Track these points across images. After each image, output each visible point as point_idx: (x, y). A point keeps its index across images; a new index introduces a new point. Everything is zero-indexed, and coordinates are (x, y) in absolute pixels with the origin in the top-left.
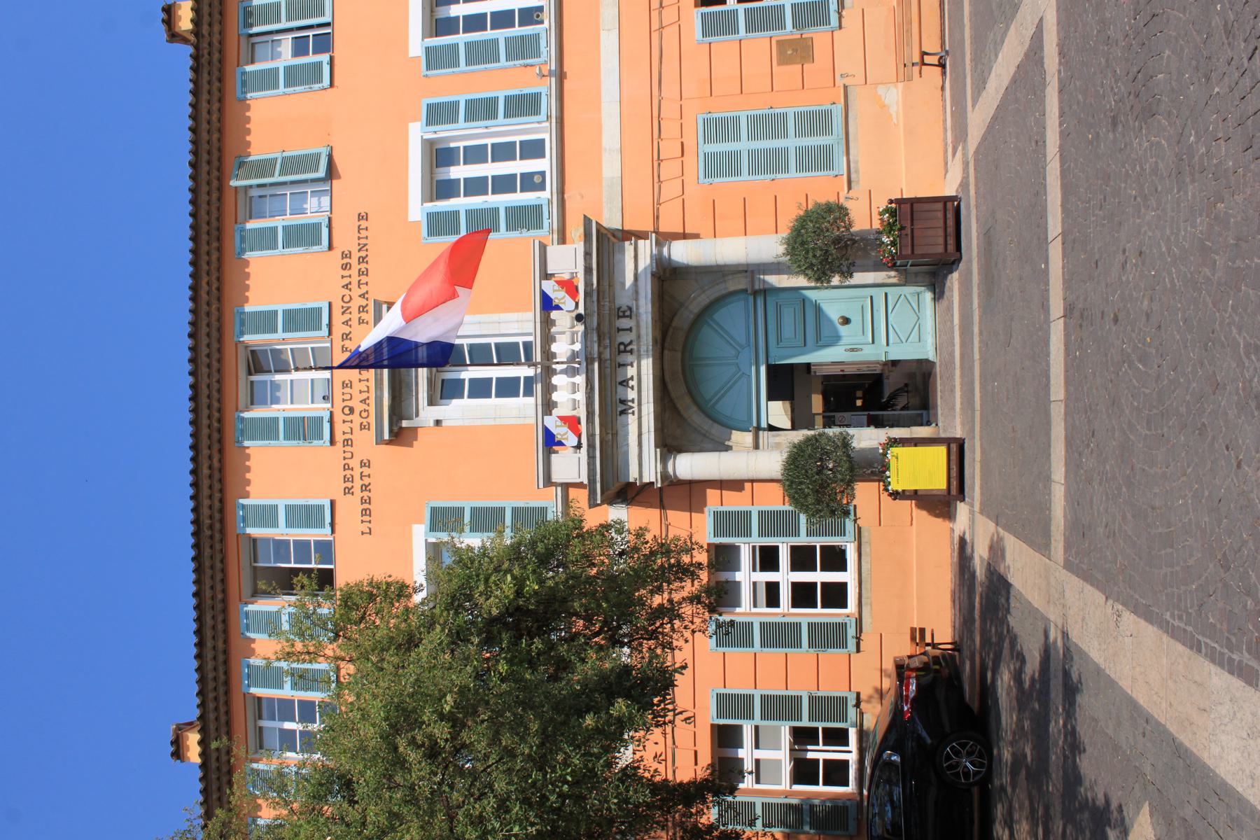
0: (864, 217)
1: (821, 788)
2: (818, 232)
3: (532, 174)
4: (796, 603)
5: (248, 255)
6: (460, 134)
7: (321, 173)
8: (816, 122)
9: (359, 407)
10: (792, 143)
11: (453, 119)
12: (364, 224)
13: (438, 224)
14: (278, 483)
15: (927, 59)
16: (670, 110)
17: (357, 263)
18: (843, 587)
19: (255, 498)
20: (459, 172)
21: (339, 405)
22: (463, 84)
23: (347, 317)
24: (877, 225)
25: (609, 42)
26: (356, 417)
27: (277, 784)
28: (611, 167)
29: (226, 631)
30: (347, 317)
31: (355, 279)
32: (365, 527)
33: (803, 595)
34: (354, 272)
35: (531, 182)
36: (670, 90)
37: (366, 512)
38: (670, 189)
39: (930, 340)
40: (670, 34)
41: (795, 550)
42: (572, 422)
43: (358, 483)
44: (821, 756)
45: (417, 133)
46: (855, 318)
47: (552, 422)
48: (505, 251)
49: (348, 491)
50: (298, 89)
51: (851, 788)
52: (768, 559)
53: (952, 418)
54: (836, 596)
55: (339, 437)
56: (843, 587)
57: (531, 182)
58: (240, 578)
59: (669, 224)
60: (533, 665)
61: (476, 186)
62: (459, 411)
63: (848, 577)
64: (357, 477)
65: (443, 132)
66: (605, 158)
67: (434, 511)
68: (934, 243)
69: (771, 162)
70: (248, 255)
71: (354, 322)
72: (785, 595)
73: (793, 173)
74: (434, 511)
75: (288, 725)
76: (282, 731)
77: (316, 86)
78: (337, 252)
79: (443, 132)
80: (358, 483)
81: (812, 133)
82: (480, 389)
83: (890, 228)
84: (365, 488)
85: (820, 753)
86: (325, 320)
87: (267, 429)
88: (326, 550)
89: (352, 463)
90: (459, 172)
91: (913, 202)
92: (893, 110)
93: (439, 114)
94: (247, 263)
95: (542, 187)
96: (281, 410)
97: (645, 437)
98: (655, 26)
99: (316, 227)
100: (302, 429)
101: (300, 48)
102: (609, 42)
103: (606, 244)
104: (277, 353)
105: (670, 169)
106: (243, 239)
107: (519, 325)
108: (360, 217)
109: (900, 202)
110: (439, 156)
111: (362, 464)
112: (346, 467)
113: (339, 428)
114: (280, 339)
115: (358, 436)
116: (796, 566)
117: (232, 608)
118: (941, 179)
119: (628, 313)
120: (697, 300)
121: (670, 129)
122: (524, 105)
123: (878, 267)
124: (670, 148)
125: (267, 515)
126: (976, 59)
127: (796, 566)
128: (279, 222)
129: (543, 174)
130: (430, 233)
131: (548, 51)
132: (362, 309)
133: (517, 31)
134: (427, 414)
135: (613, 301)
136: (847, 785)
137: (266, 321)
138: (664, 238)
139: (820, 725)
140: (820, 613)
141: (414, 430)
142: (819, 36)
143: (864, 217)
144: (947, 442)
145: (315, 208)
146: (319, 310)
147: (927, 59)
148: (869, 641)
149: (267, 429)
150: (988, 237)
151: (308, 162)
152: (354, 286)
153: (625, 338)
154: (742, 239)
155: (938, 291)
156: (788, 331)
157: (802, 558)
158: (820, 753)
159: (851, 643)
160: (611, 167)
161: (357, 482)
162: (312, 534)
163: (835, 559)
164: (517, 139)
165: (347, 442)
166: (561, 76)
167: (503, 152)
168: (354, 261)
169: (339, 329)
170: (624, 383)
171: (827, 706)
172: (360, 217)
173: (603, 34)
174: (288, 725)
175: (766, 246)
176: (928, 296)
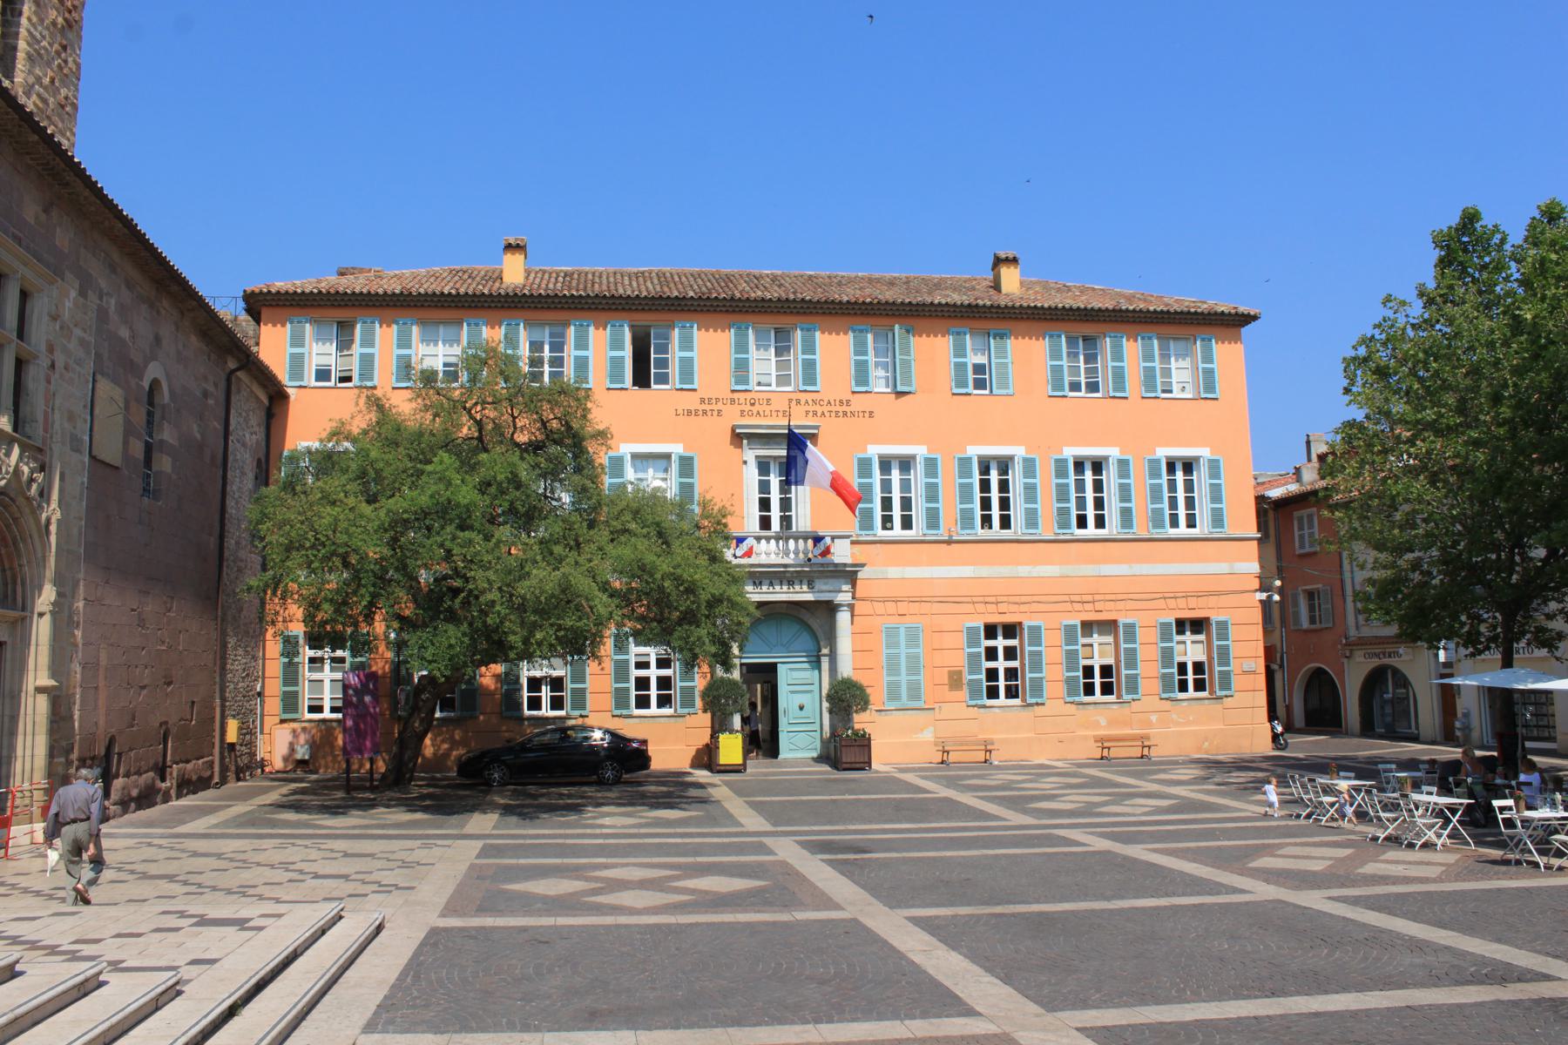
0: (861, 721)
1: (526, 694)
2: (854, 696)
4: (638, 679)
5: (851, 334)
6: (918, 477)
7: (900, 388)
8: (914, 692)
9: (755, 409)
10: (904, 678)
11: (927, 475)
13: (864, 466)
14: (703, 349)
16: (926, 607)
17: (843, 410)
18: (648, 706)
19: (698, 335)
20: (896, 476)
21: (756, 396)
22: (948, 481)
24: (857, 726)
25: (967, 571)
26: (748, 407)
27: (511, 341)
28: (894, 572)
31: (834, 409)
33: (643, 683)
36: (937, 608)
37: (689, 412)
38: (879, 608)
42: (749, 554)
44: (543, 694)
45: (920, 451)
46: (803, 713)
47: (750, 541)
48: (845, 521)
49: (702, 401)
51: (527, 712)
52: (1010, 653)
53: (758, 767)
54: (643, 702)
55: (736, 396)
56: (648, 706)
57: (887, 521)
58: (643, 319)
59: (860, 607)
61: (887, 486)
62: (752, 474)
63: (654, 709)
65: (920, 467)
66: (899, 569)
67: (691, 459)
68: (848, 756)
69: (893, 668)
70: (851, 334)
72: (642, 673)
73: (886, 678)
74: (691, 459)
75: (547, 348)
76: (542, 344)
78: (850, 397)
79: (920, 467)
81: (909, 689)
82: (764, 487)
83: (856, 733)
84: (705, 412)
85: (545, 693)
87: (742, 347)
88: (663, 379)
90: (896, 476)
91: (869, 746)
93: (931, 465)
94: (846, 333)
95: (884, 528)
96: (754, 354)
99: (866, 383)
100: (742, 368)
101: (979, 369)
102: (967, 571)
103: (849, 574)
104: (788, 349)
105: (891, 607)
106: (861, 331)
107: (803, 519)
109: (869, 739)
110: (906, 464)
113: (742, 396)
114: (797, 356)
115: (737, 408)
116: (659, 679)
117: (624, 314)
118: (882, 759)
120: (815, 623)
121: (914, 608)
122: (933, 520)
123: (832, 726)
124: (903, 608)
125: (687, 344)
126: (1004, 798)
127: (659, 679)
128: (871, 357)
131: (965, 535)
132: (815, 413)
133: (978, 513)
134: (750, 455)
137: (809, 347)
138: (851, 607)
141: (741, 446)
142: (964, 694)
143: (861, 721)
144: (744, 765)
145: (879, 381)
149: (742, 347)
150: (853, 780)
151: (907, 381)
154: (849, 654)
155: (820, 759)
156: (796, 674)
157: (664, 683)
158: (545, 693)
159: (618, 712)
160: (894, 572)
161: (707, 408)
162: (674, 370)
163: (664, 701)
164: (913, 513)
165: (733, 401)
166: (949, 542)
169: (803, 397)
170: (771, 584)
171: (579, 699)
174: (547, 348)
175: (846, 669)
176: (815, 755)
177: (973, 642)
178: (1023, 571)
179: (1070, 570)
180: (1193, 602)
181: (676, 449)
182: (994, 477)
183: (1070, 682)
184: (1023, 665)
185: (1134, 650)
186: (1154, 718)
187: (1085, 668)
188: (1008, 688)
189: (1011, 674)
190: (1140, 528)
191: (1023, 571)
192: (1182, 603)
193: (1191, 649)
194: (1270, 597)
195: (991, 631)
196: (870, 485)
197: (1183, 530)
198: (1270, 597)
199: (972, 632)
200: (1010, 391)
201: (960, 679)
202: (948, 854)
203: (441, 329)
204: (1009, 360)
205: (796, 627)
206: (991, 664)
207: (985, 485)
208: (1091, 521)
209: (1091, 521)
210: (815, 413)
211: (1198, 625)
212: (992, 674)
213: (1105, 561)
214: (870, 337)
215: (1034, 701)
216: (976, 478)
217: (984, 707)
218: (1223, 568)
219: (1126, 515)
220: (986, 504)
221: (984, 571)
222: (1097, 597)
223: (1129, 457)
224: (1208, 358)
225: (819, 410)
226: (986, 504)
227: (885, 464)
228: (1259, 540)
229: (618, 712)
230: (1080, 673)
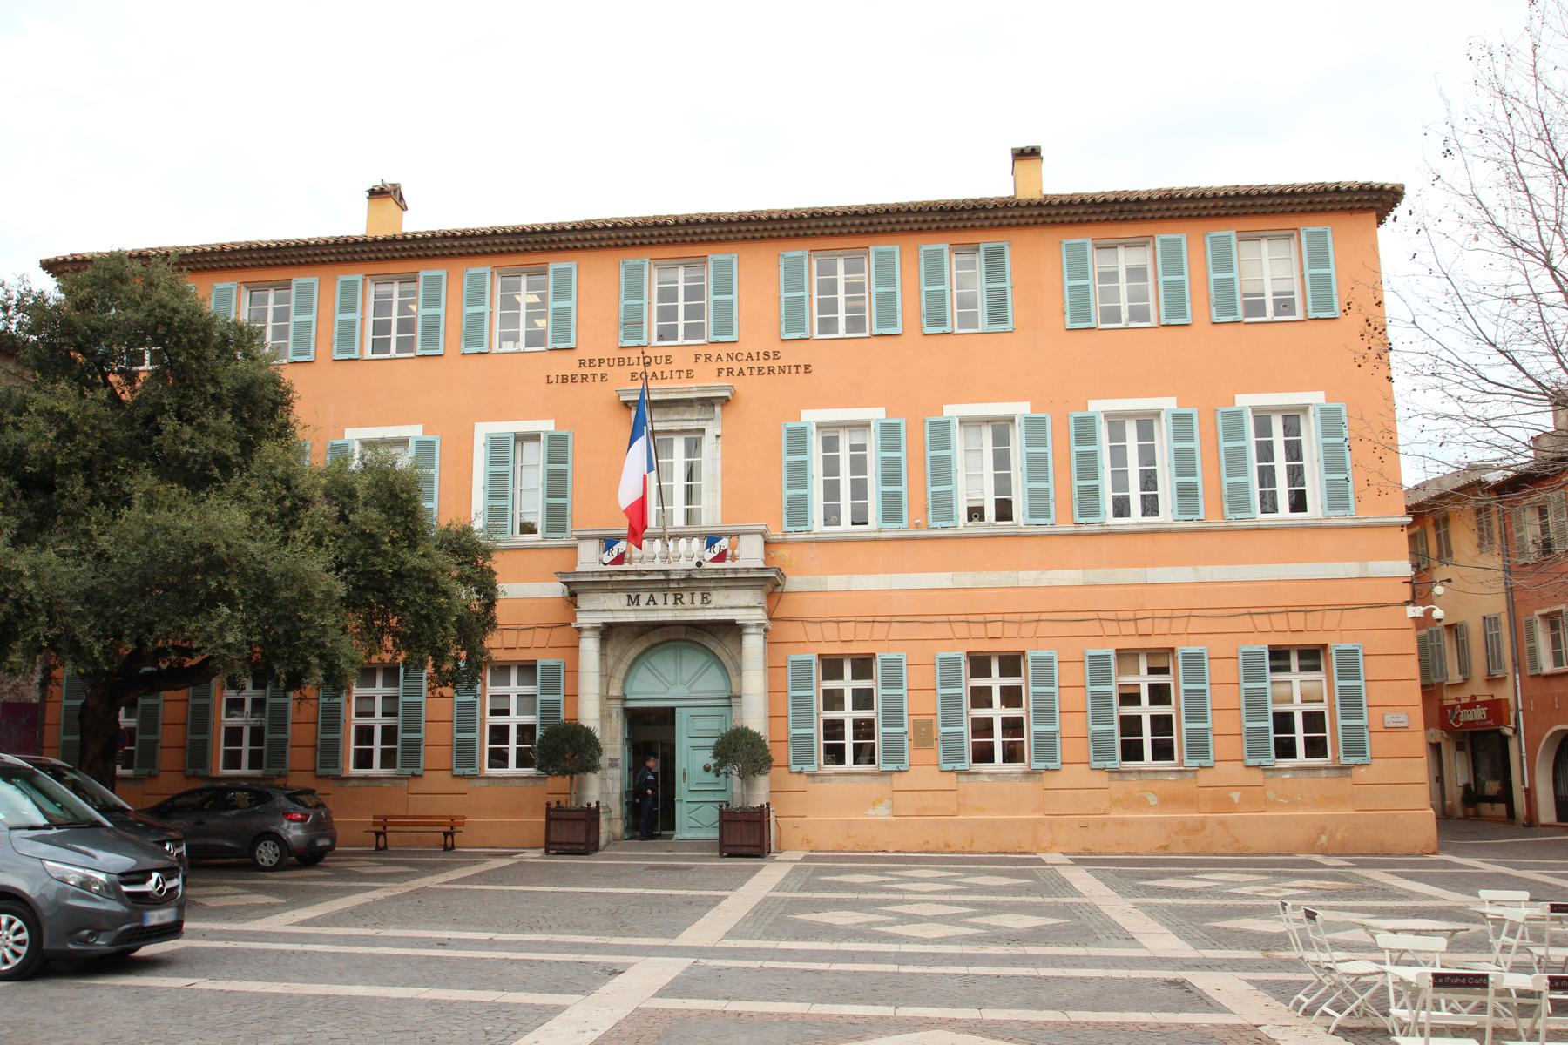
1: (353, 747)
3: (838, 514)
4: (1124, 719)
12: (801, 370)
15: (381, 844)
17: (769, 365)
23: (724, 357)
25: (943, 580)
28: (835, 582)
29: (469, 255)
30: (724, 357)
31: (756, 364)
32: (553, 378)
34: (762, 363)
35: (832, 516)
37: (565, 379)
39: (689, 835)
40: (1095, 628)
41: (870, 723)
43: (588, 371)
49: (582, 363)
50: (924, 304)
52: (1012, 697)
55: (624, 354)
56: (990, 759)
57: (832, 516)
60: (86, 533)
64: (594, 371)
67: (565, 438)
71: (720, 365)
72: (499, 720)
77: (924, 321)
80: (588, 371)
86: (885, 331)
89: (605, 365)
92: (871, 812)
97: (610, 615)
98: (1102, 615)
102: (943, 580)
108: (807, 367)
110: (1146, 424)
111: (603, 376)
112: (601, 361)
117: (487, 260)
119: (705, 601)
129: (838, 523)
130: (789, 430)
133: (1255, 490)
135: (715, 588)
136: (225, 767)
139: (265, 748)
140: (819, 743)
146: (1184, 315)
147: (381, 844)
148: (462, 785)
152: (750, 363)
153: (687, 598)
156: (700, 724)
160: (835, 582)
163: (1012, 754)
167: (859, 489)
168: (771, 363)
172: (807, 367)
173: (949, 575)
177: (950, 678)
178: (1027, 578)
179: (1100, 576)
180: (1297, 621)
181: (546, 426)
182: (1278, 439)
183: (1100, 740)
184: (1332, 707)
185: (1051, 696)
186: (1236, 796)
187: (1125, 720)
188: (858, 749)
189: (1013, 726)
190: (1206, 514)
191: (1027, 578)
192: (1279, 622)
193: (1297, 691)
194: (1428, 613)
195: (979, 664)
196: (1242, 450)
197: (1136, 517)
198: (1428, 613)
199: (949, 666)
200: (1009, 327)
201: (930, 732)
202: (359, 990)
203: (1264, 244)
204: (1007, 284)
205: (701, 659)
206: (1013, 712)
207: (1266, 452)
208: (1136, 506)
209: (1136, 506)
210: (730, 371)
211: (1312, 656)
212: (983, 728)
213: (1154, 563)
214: (841, 264)
215: (1042, 765)
216: (1251, 441)
217: (967, 773)
218: (1350, 569)
219: (1186, 495)
220: (1267, 476)
221: (967, 579)
222: (1140, 614)
223: (1194, 411)
224: (1319, 259)
225: (736, 366)
226: (1267, 476)
227: (1116, 423)
228: (1409, 526)
229: (1252, 762)
230: (1270, 724)
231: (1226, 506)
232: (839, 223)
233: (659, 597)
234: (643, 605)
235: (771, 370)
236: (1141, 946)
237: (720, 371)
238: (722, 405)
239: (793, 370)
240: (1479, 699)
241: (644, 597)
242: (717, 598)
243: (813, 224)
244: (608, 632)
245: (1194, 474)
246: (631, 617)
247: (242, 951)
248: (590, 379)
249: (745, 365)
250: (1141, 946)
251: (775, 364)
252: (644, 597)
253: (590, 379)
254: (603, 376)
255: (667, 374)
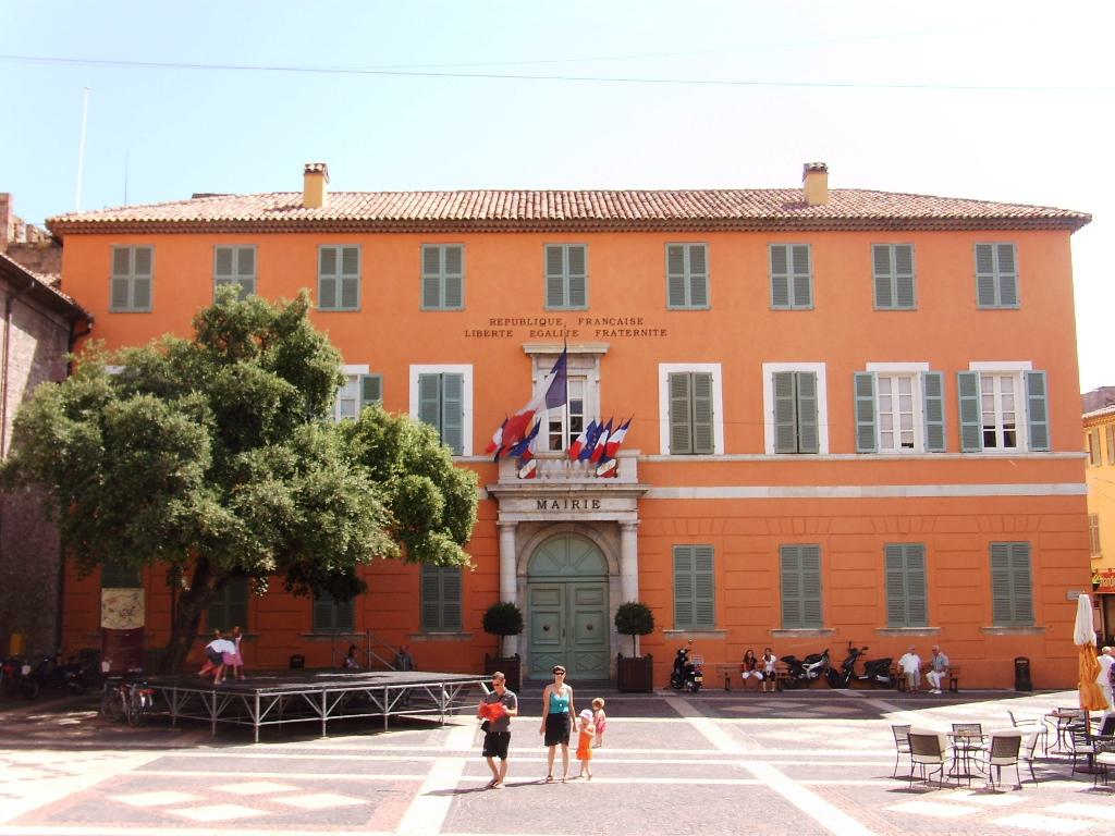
15: (953, 683)
23: (601, 321)
30: (601, 321)
31: (624, 327)
32: (470, 332)
34: (629, 327)
37: (479, 334)
67: (377, 380)
71: (596, 327)
89: (510, 324)
97: (524, 515)
108: (663, 332)
112: (507, 321)
119: (596, 505)
160: (684, 493)
208: (1000, 439)
231: (962, 442)
232: (491, 224)
233: (561, 503)
234: (548, 508)
235: (636, 332)
236: (716, 749)
237: (598, 332)
238: (600, 358)
239: (653, 333)
240: (1100, 571)
241: (550, 503)
242: (605, 503)
243: (742, 223)
244: (519, 527)
245: (940, 419)
246: (540, 517)
247: (184, 779)
248: (499, 334)
249: (617, 328)
250: (716, 749)
251: (640, 328)
252: (550, 503)
253: (499, 334)
254: (509, 332)
255: (557, 332)
